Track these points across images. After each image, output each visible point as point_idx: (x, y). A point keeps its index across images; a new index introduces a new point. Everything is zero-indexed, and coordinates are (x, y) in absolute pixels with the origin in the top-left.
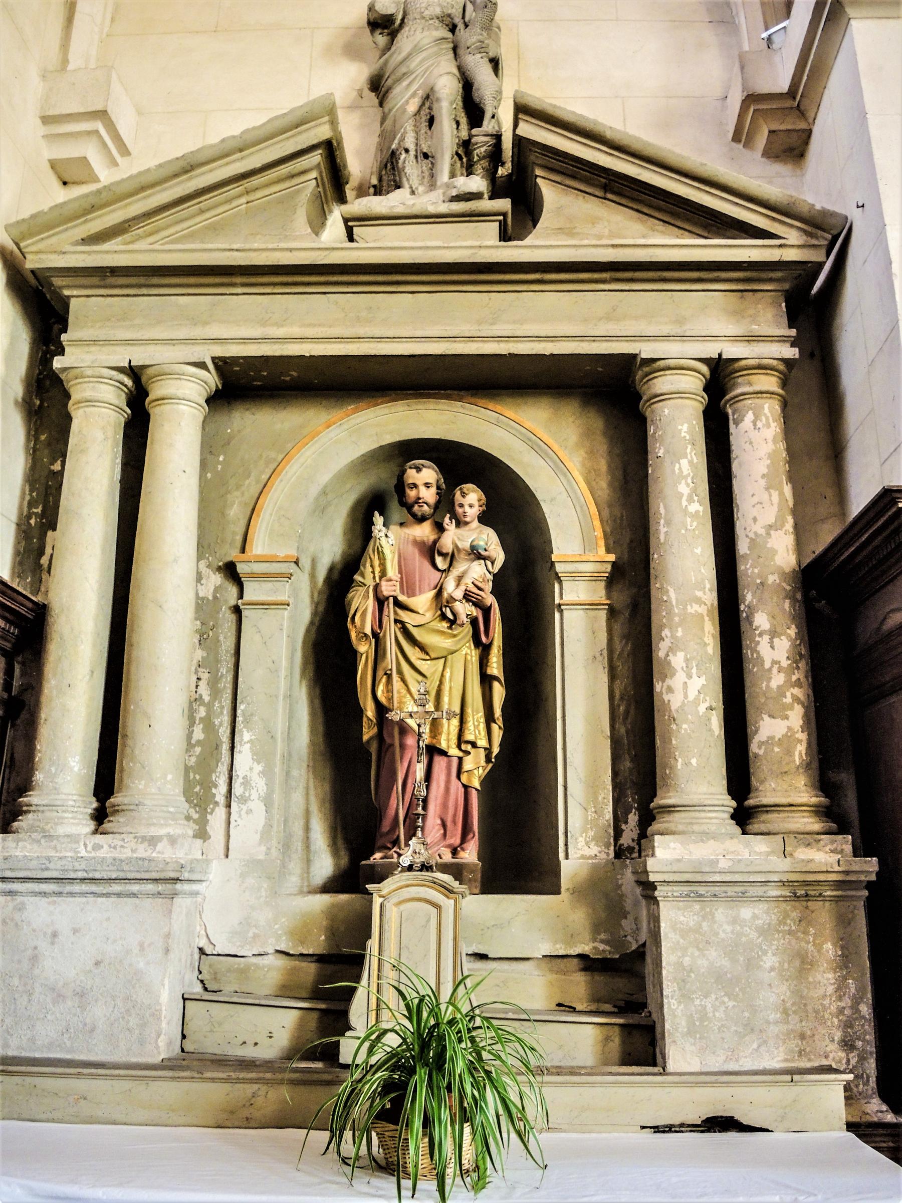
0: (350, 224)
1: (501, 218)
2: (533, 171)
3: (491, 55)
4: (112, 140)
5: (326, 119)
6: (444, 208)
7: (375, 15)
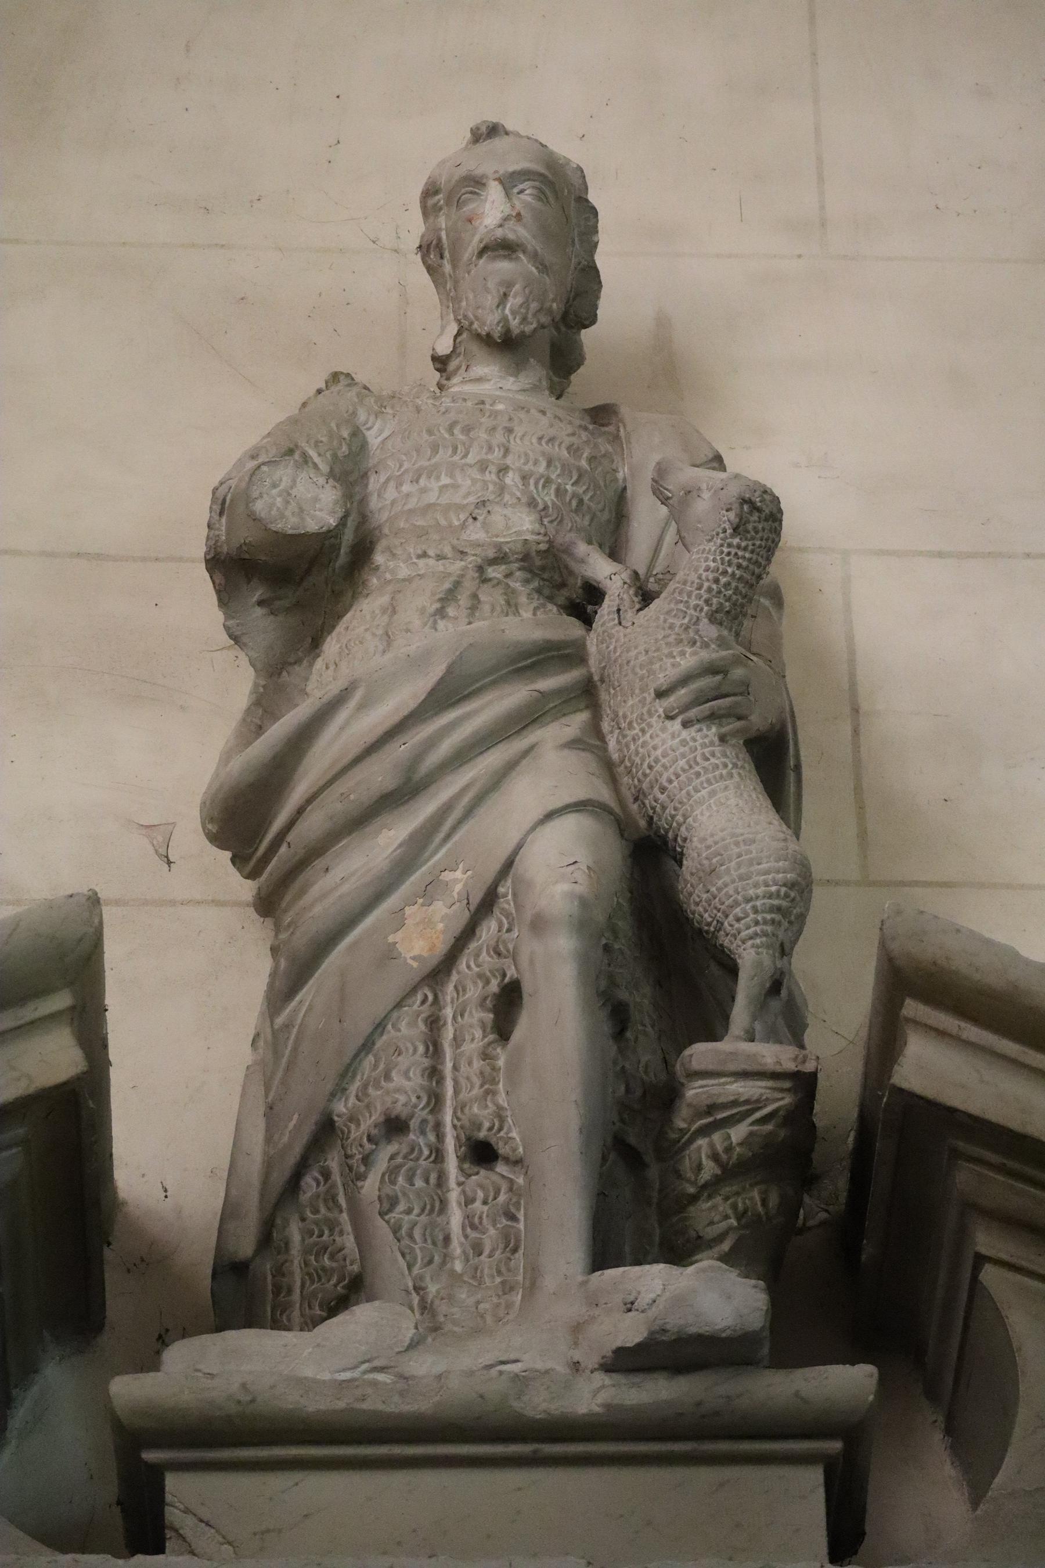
0: (150, 1456)
1: (836, 1446)
2: (963, 1234)
3: (759, 720)
4: (366, 1456)
5: (61, 1001)
6: (592, 1395)
7: (246, 534)
